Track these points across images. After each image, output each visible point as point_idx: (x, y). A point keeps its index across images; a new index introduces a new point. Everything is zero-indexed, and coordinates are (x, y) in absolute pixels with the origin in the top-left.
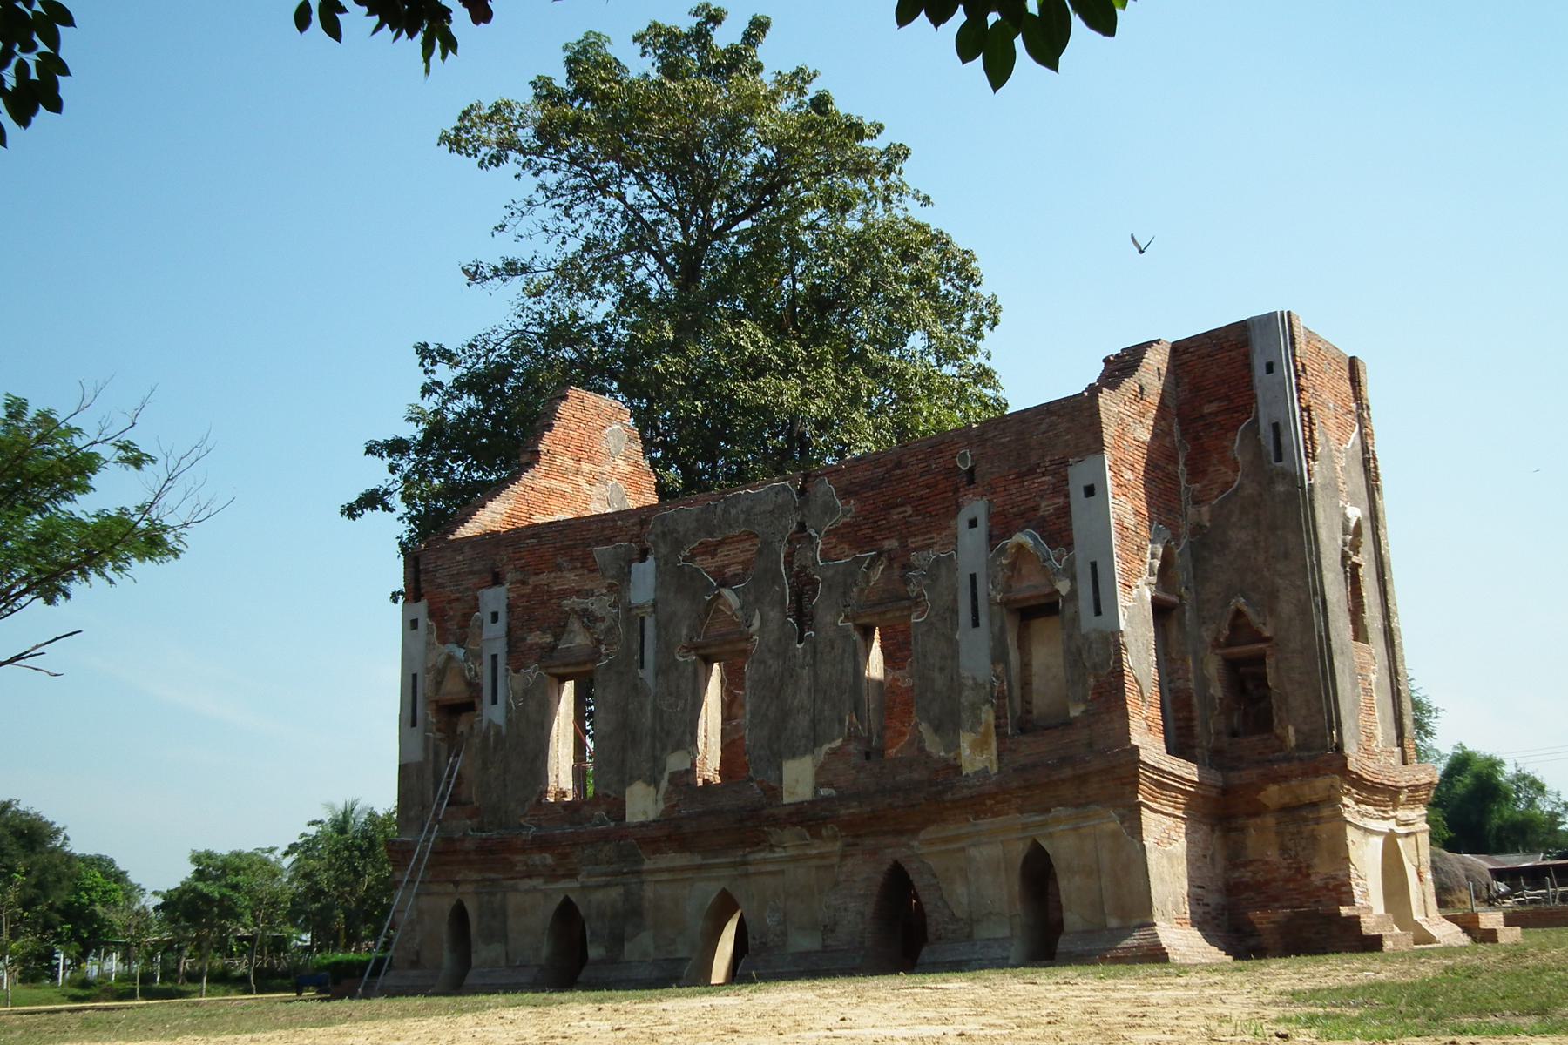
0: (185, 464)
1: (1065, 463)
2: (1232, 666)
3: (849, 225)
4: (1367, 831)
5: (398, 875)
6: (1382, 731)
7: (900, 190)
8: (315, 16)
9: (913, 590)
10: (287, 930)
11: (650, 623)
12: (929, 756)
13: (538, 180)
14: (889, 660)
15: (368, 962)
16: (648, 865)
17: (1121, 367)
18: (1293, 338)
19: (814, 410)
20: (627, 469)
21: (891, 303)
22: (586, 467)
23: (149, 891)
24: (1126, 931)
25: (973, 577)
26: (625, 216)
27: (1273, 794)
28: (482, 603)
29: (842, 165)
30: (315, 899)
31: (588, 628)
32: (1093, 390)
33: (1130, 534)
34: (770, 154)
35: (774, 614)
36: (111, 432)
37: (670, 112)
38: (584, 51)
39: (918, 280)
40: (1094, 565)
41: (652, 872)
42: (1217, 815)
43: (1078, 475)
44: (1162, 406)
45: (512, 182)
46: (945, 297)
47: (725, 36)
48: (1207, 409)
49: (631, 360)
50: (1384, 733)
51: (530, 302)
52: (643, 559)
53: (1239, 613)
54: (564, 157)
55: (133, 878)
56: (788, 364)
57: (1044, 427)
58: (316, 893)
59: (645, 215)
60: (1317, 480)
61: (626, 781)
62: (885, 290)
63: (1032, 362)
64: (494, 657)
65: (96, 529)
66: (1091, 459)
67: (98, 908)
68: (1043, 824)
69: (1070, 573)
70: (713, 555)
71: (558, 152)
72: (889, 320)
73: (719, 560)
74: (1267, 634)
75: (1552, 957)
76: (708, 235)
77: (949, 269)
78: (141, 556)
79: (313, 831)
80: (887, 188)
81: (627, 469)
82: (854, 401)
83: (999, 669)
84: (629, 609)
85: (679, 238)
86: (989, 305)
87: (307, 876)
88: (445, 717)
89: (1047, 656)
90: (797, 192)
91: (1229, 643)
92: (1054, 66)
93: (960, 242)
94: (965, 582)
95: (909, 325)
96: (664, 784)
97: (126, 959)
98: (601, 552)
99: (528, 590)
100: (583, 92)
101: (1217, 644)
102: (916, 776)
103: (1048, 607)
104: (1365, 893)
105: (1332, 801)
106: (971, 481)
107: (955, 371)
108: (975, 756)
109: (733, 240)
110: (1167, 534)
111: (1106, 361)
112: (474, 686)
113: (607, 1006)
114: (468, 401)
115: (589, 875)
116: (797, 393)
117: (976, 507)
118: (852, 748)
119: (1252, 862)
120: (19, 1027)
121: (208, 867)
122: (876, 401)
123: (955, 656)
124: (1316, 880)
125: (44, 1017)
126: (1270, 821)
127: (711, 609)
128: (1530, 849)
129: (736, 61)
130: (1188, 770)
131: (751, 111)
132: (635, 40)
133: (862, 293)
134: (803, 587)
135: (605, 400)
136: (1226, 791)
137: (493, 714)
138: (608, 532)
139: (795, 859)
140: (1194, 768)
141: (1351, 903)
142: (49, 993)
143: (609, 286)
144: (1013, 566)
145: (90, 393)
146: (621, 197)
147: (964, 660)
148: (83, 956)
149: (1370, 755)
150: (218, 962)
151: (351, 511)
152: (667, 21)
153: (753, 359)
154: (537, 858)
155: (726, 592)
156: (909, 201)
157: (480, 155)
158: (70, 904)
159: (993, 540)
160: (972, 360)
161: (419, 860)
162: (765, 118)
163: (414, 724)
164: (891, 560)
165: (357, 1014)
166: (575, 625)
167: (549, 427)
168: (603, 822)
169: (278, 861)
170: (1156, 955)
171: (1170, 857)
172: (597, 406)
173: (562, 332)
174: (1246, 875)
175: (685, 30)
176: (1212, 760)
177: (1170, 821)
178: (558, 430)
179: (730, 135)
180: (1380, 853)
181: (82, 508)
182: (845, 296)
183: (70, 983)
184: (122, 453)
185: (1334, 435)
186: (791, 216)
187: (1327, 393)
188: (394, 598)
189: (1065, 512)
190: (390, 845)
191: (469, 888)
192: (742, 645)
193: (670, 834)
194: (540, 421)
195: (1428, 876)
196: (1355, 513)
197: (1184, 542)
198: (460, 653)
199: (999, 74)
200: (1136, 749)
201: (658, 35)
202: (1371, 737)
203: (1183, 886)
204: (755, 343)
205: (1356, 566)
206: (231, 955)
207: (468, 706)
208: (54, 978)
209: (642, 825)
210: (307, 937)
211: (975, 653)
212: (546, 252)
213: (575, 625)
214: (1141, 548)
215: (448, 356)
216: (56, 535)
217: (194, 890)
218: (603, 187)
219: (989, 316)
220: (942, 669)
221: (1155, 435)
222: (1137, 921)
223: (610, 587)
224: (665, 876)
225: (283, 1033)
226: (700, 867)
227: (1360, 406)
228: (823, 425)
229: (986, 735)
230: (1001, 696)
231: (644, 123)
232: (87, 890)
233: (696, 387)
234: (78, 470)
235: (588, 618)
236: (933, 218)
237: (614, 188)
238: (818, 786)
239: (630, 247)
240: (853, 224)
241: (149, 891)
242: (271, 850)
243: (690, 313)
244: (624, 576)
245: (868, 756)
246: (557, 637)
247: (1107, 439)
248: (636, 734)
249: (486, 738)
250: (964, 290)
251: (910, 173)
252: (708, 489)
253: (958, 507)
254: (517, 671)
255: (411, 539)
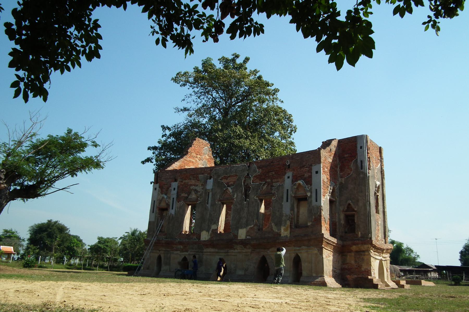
0: (107, 147)
1: (311, 165)
2: (347, 216)
3: (263, 106)
4: (376, 259)
5: (146, 247)
6: (381, 235)
7: (276, 99)
8: (160, 42)
9: (273, 192)
10: (117, 257)
11: (210, 194)
12: (273, 231)
13: (193, 90)
14: (266, 208)
15: (137, 266)
16: (205, 250)
17: (326, 144)
18: (367, 141)
19: (252, 148)
20: (208, 158)
21: (272, 125)
22: (199, 156)
23: (87, 245)
24: (317, 277)
25: (288, 190)
26: (212, 99)
27: (354, 248)
28: (171, 185)
29: (263, 92)
30: (125, 250)
31: (196, 194)
32: (319, 149)
33: (325, 183)
34: (247, 88)
35: (240, 194)
36: (91, 138)
37: (225, 77)
38: (206, 62)
39: (279, 120)
40: (316, 190)
41: (205, 252)
42: (340, 252)
43: (314, 169)
44: (335, 154)
45: (187, 90)
46: (284, 124)
47: (239, 61)
48: (346, 156)
49: (211, 132)
50: (381, 236)
51: (189, 118)
52: (210, 179)
53: (349, 204)
54: (200, 85)
55: (84, 241)
56: (247, 137)
57: (307, 156)
58: (125, 249)
59: (217, 100)
60: (370, 175)
61: (201, 230)
62: (271, 122)
63: (304, 141)
64: (173, 198)
65: (85, 160)
66: (318, 165)
67: (75, 248)
68: (299, 250)
69: (311, 191)
70: (227, 179)
71: (198, 84)
72: (271, 129)
73: (228, 181)
74: (356, 210)
75: (426, 295)
76: (231, 106)
77: (286, 118)
78: (95, 168)
79: (126, 234)
80: (273, 98)
81: (208, 158)
82: (262, 147)
83: (292, 212)
84: (206, 190)
85: (224, 105)
86: (294, 127)
87: (124, 245)
88: (159, 210)
89: (303, 210)
90: (252, 98)
91: (346, 211)
92: (354, 66)
93: (289, 112)
94: (285, 191)
95: (275, 130)
96: (210, 232)
97: (80, 260)
98: (201, 176)
99: (183, 183)
100: (206, 71)
101: (343, 211)
102: (270, 235)
103: (305, 199)
104: (374, 273)
105: (368, 251)
106: (289, 168)
107: (285, 142)
108: (285, 232)
109: (237, 107)
110: (334, 184)
111: (323, 142)
112: (168, 205)
113: (195, 284)
114: (172, 139)
115: (191, 252)
116: (249, 144)
117: (290, 174)
118: (256, 227)
119: (347, 263)
120: (55, 276)
121: (101, 240)
122: (266, 147)
123: (282, 208)
124: (363, 269)
125: (62, 273)
126: (353, 254)
127: (225, 192)
128: (409, 265)
129: (241, 67)
130: (335, 240)
131: (244, 78)
132: (218, 60)
133: (265, 122)
134: (247, 188)
135: (204, 141)
136: (343, 246)
137: (172, 212)
138: (203, 172)
139: (239, 253)
140: (336, 240)
141: (371, 275)
142: (62, 266)
143: (207, 115)
144: (297, 188)
145: (87, 129)
146: (212, 95)
147: (284, 209)
148: (70, 259)
149: (378, 241)
150: (101, 263)
151: (143, 162)
152: (226, 56)
153: (239, 135)
154: (179, 246)
155: (229, 188)
156: (278, 102)
157: (180, 84)
158: (69, 246)
159: (293, 181)
160: (289, 140)
161: (151, 244)
162: (247, 80)
163: (153, 212)
164: (268, 184)
165: (135, 280)
166: (193, 193)
167: (191, 146)
168: (195, 239)
169: (117, 241)
170: (324, 284)
171: (329, 260)
172: (202, 142)
173: (195, 125)
174: (346, 266)
175: (230, 59)
176: (340, 238)
177: (329, 252)
178: (193, 147)
179: (238, 83)
180: (378, 264)
181: (82, 155)
182: (261, 122)
183: (67, 264)
184: (93, 144)
185: (375, 164)
186: (251, 103)
187: (374, 155)
188: (151, 183)
189: (310, 177)
190: (145, 240)
191: (163, 252)
192: (232, 201)
193: (211, 244)
194: (189, 145)
195: (389, 271)
196: (378, 183)
197: (338, 186)
198: (165, 197)
199: (339, 66)
200: (323, 234)
201: (224, 59)
202: (378, 236)
203: (331, 268)
204: (240, 131)
205: (378, 196)
206: (104, 261)
207: (166, 209)
208: (63, 263)
209: (204, 241)
210: (122, 259)
211: (286, 208)
212: (194, 106)
213: (193, 193)
214: (328, 187)
215: (169, 129)
216: (75, 161)
217: (98, 246)
218: (208, 93)
219: (294, 130)
220: (278, 211)
221: (333, 161)
222: (319, 275)
223: (202, 185)
224: (209, 254)
225: (118, 284)
226: (217, 252)
227: (381, 158)
228: (254, 151)
229: (287, 228)
230: (292, 219)
231: (219, 79)
232: (73, 243)
233: (225, 140)
234: (83, 146)
235: (196, 191)
236: (283, 106)
237: (210, 93)
238: (247, 236)
239: (213, 107)
240: (265, 106)
241: (87, 245)
242: (116, 238)
243: (225, 123)
244: (206, 182)
245: (259, 230)
246: (189, 195)
247: (322, 161)
248: (205, 220)
249: (170, 217)
250: (289, 123)
251: (279, 95)
252: (225, 164)
253: (285, 173)
254: (178, 202)
255: (156, 169)
